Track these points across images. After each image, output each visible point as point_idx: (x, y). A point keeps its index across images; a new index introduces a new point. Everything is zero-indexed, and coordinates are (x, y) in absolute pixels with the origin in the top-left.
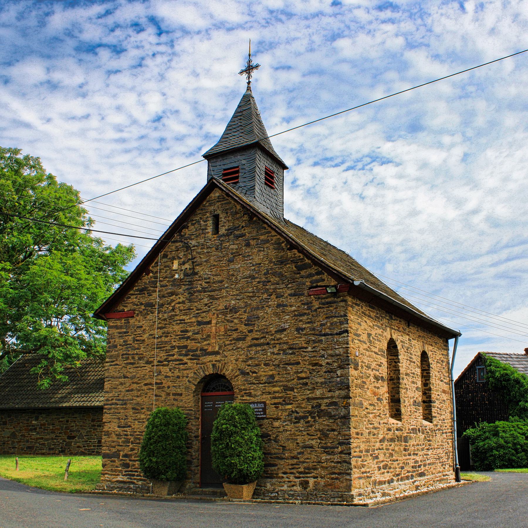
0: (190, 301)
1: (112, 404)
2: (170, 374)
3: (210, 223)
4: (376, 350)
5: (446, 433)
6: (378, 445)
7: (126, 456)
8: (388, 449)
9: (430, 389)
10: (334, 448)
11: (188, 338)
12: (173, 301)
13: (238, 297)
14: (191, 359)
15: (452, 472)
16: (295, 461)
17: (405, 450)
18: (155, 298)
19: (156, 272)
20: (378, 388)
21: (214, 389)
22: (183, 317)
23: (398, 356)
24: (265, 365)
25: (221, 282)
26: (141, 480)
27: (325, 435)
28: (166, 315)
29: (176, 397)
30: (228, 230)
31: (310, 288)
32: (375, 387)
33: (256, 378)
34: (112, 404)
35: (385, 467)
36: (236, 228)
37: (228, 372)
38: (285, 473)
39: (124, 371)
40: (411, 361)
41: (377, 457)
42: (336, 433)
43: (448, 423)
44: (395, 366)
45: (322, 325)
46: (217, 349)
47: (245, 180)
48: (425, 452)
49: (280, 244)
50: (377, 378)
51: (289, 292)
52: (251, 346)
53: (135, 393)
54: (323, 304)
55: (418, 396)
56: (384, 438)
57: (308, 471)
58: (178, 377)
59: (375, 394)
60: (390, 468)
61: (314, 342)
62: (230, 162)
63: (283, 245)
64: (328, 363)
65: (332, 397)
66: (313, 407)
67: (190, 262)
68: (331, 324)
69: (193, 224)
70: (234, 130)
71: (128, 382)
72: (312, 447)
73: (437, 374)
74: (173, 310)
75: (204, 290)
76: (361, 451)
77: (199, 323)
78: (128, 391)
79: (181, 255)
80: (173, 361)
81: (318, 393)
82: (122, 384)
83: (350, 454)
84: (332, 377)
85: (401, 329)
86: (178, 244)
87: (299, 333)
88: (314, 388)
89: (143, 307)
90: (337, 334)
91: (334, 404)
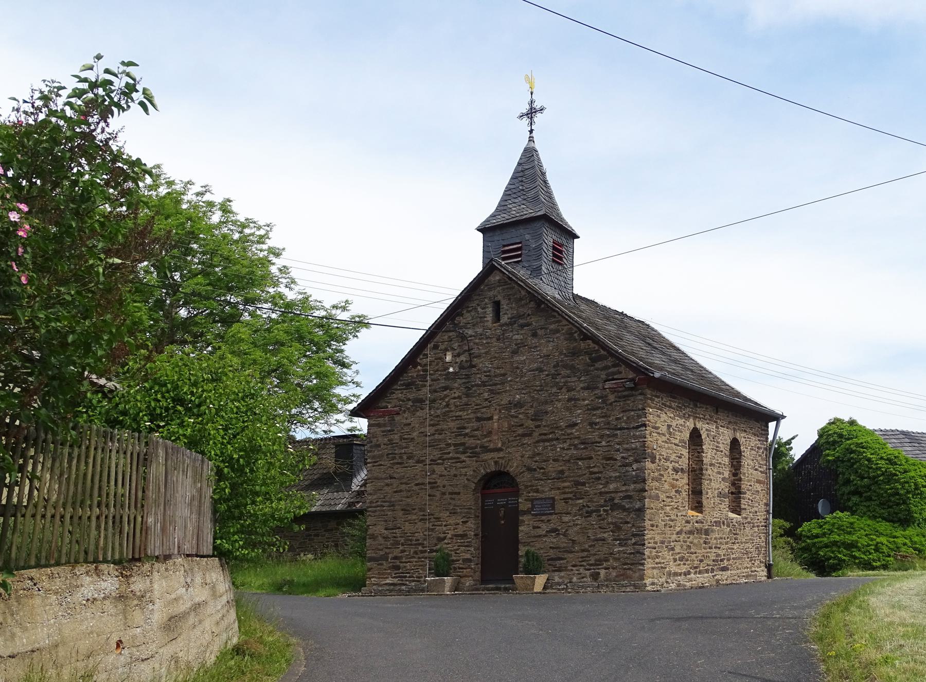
0: (468, 396)
1: (378, 506)
2: (445, 473)
3: (490, 310)
4: (677, 442)
5: (758, 526)
6: (674, 537)
7: (396, 558)
8: (685, 542)
9: (740, 480)
10: (627, 540)
11: (467, 434)
12: (446, 396)
13: (524, 391)
14: (469, 457)
15: (763, 568)
16: (586, 553)
17: (705, 543)
18: (426, 392)
19: (426, 365)
20: (677, 480)
21: (495, 486)
22: (457, 414)
23: (701, 445)
24: (554, 460)
25: (504, 375)
26: (414, 581)
27: (617, 528)
28: (439, 412)
29: (453, 496)
30: (511, 318)
31: (605, 381)
32: (673, 479)
33: (543, 473)
34: (378, 506)
35: (681, 559)
36: (520, 316)
37: (513, 468)
38: (574, 566)
39: (390, 471)
40: (717, 451)
41: (673, 549)
42: (629, 525)
43: (761, 516)
44: (698, 457)
45: (617, 419)
46: (500, 445)
47: (529, 258)
48: (729, 546)
49: (571, 334)
50: (676, 470)
51: (582, 385)
52: (538, 442)
53: (404, 494)
54: (620, 397)
55: (725, 487)
56: (681, 530)
57: (599, 563)
58: (455, 476)
59: (673, 486)
60: (687, 560)
61: (609, 436)
62: (512, 236)
63: (576, 335)
64: (623, 457)
65: (626, 491)
66: (605, 501)
67: (467, 354)
68: (628, 418)
69: (469, 312)
70: (515, 196)
71: (395, 483)
72: (604, 540)
73: (751, 462)
74: (447, 405)
75: (484, 384)
76: (656, 543)
77: (479, 419)
78: (396, 492)
79: (456, 345)
80: (448, 459)
81: (612, 487)
82: (387, 485)
83: (644, 545)
84: (627, 471)
85: (707, 417)
86: (451, 334)
87: (592, 428)
88: (608, 483)
89: (410, 403)
90: (634, 428)
91: (629, 497)
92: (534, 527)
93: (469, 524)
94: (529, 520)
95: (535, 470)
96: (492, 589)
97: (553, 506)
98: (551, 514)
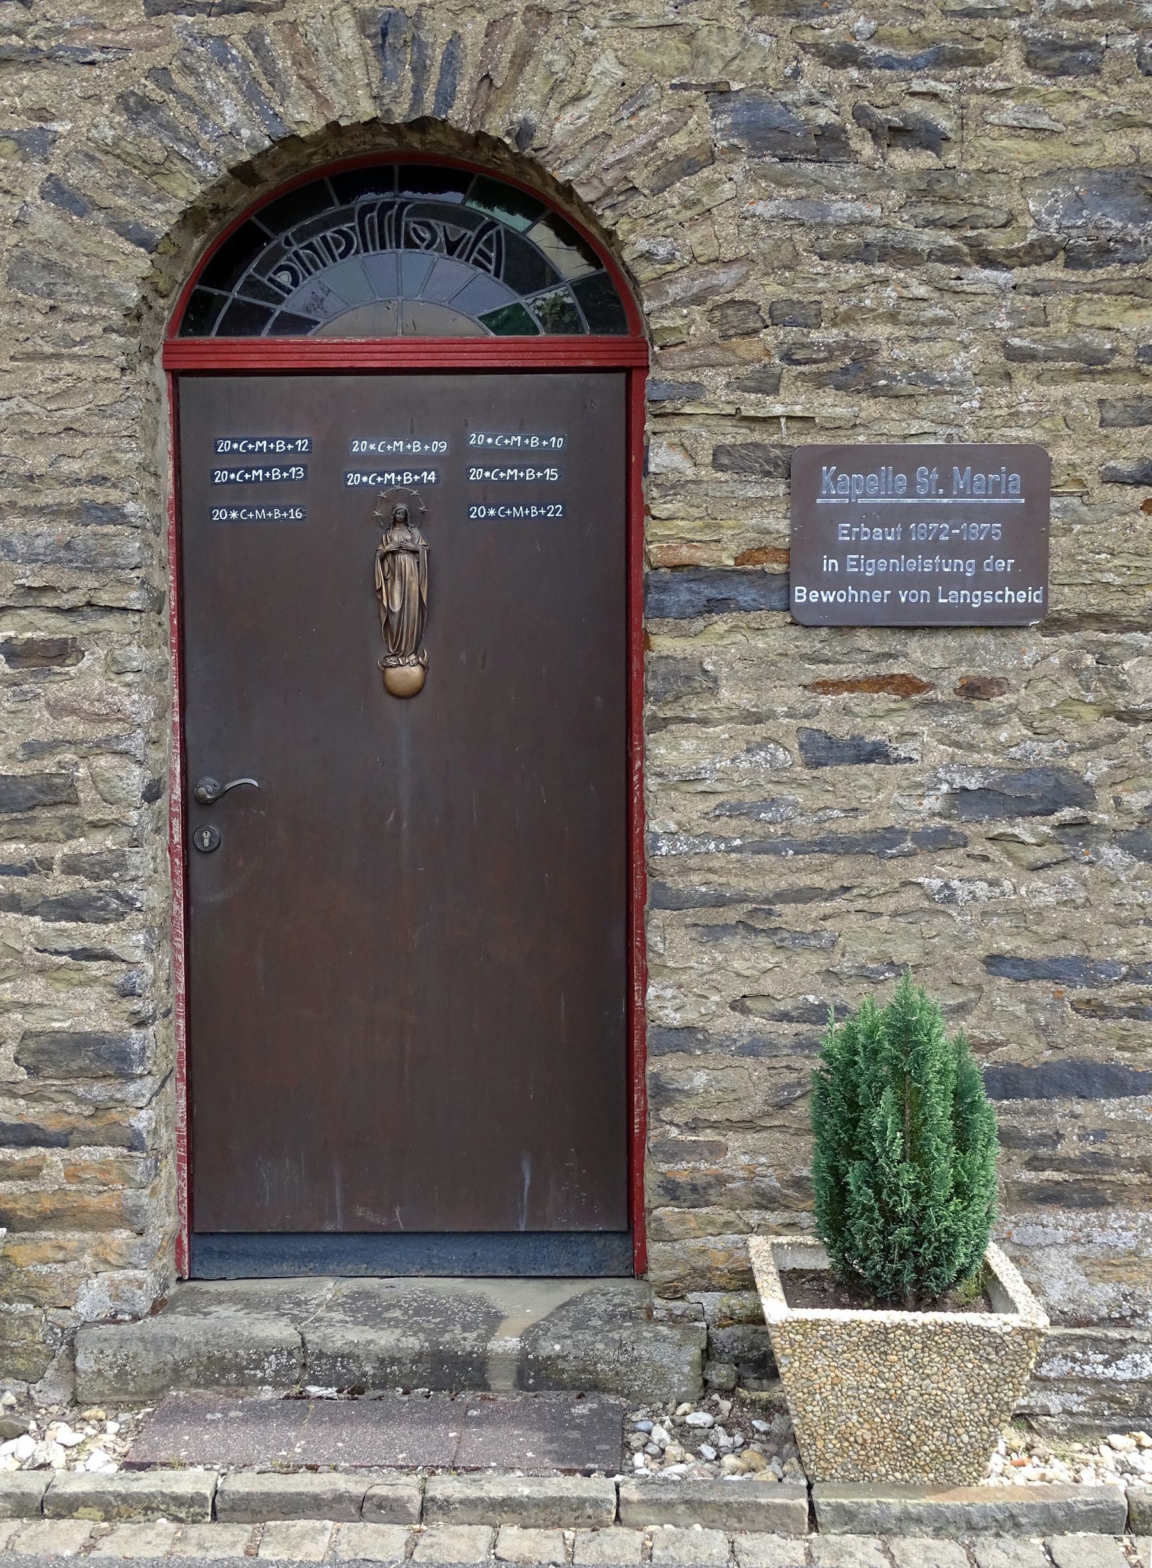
33: (926, 189)
92: (822, 751)
93: (86, 677)
94: (766, 669)
95: (829, 143)
96: (362, 1386)
97: (1028, 540)
98: (1002, 623)
